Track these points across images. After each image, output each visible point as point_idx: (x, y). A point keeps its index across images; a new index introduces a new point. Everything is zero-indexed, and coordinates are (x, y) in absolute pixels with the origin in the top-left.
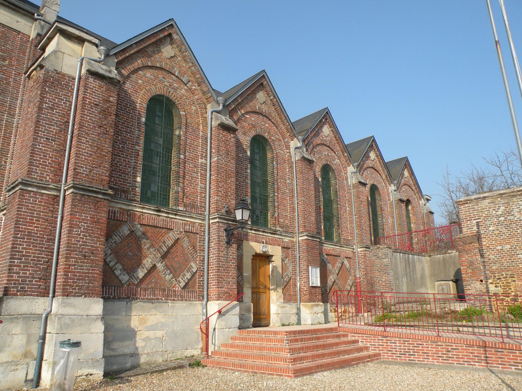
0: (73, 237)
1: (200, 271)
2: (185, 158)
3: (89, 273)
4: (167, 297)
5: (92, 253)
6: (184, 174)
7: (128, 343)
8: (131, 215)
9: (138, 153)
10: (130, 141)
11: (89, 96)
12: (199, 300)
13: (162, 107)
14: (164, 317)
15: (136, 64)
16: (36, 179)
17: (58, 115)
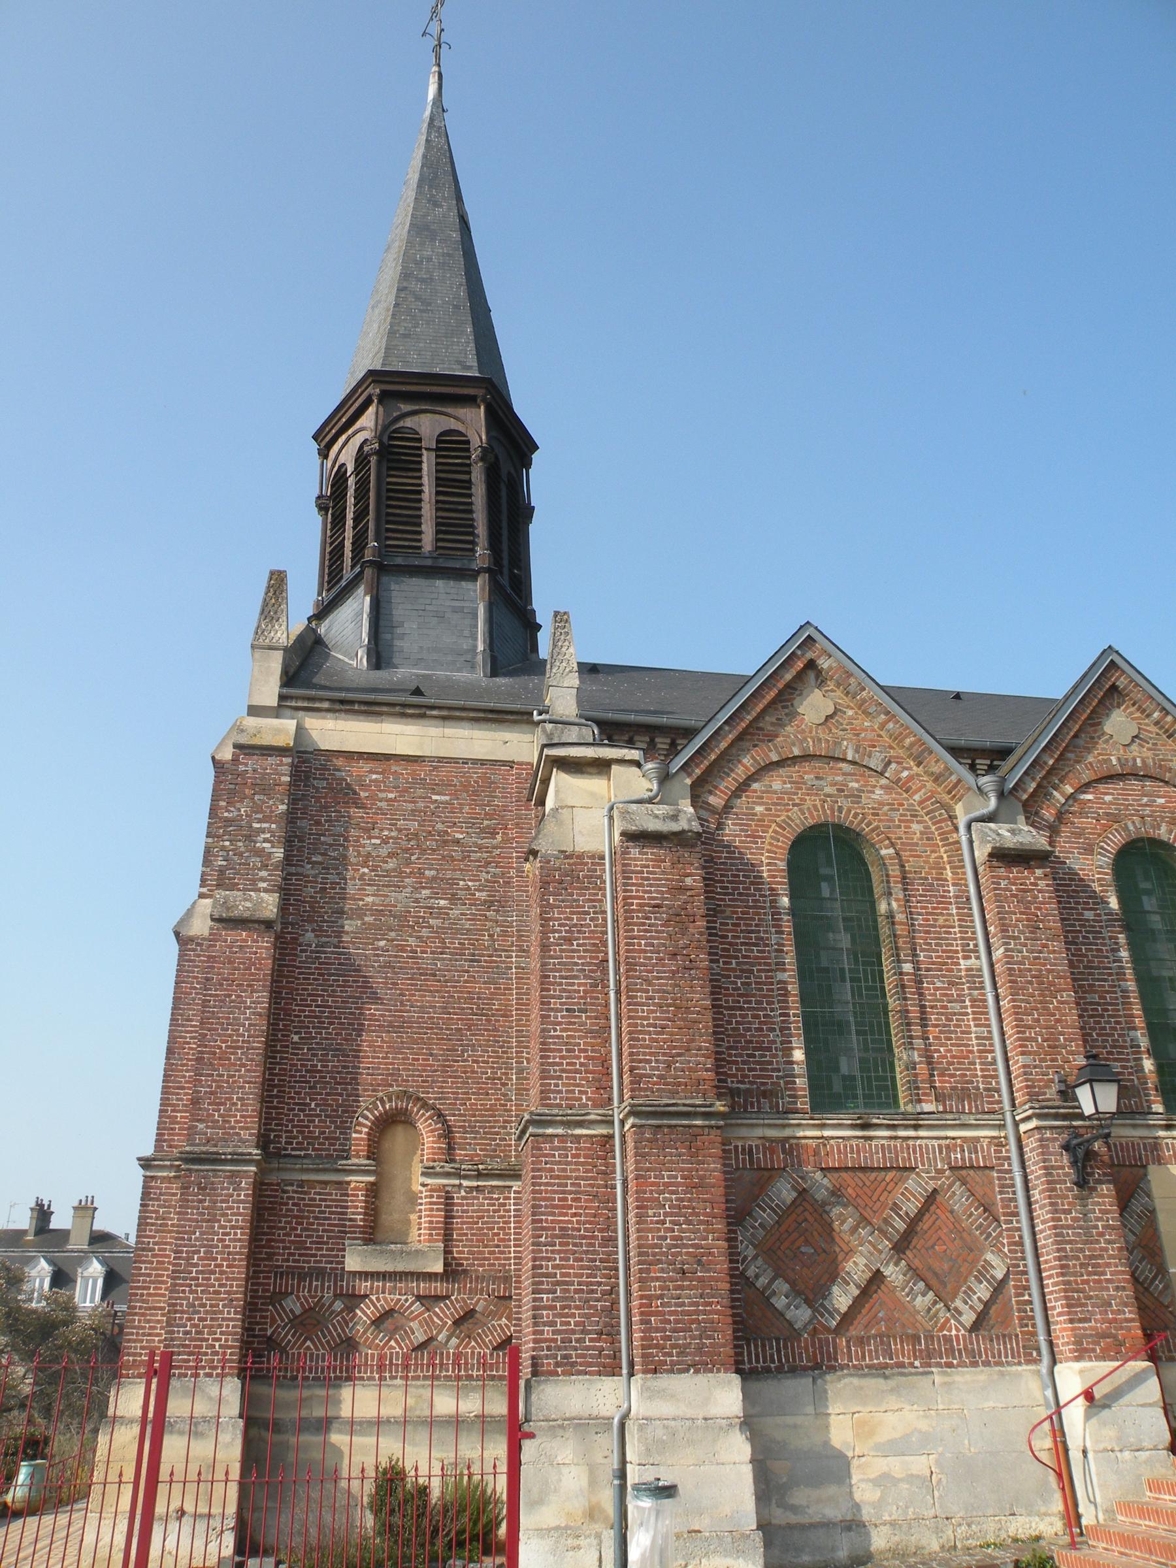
0: (650, 1230)
1: (1018, 1273)
2: (919, 969)
3: (697, 1313)
4: (928, 1358)
5: (699, 1262)
6: (923, 1013)
7: (832, 1490)
8: (790, 1148)
9: (786, 989)
10: (760, 964)
11: (637, 891)
12: (1028, 1362)
13: (830, 855)
14: (926, 1417)
15: (740, 770)
16: (559, 1106)
17: (585, 951)
